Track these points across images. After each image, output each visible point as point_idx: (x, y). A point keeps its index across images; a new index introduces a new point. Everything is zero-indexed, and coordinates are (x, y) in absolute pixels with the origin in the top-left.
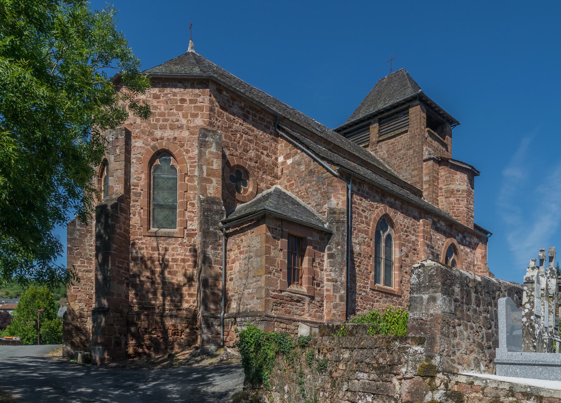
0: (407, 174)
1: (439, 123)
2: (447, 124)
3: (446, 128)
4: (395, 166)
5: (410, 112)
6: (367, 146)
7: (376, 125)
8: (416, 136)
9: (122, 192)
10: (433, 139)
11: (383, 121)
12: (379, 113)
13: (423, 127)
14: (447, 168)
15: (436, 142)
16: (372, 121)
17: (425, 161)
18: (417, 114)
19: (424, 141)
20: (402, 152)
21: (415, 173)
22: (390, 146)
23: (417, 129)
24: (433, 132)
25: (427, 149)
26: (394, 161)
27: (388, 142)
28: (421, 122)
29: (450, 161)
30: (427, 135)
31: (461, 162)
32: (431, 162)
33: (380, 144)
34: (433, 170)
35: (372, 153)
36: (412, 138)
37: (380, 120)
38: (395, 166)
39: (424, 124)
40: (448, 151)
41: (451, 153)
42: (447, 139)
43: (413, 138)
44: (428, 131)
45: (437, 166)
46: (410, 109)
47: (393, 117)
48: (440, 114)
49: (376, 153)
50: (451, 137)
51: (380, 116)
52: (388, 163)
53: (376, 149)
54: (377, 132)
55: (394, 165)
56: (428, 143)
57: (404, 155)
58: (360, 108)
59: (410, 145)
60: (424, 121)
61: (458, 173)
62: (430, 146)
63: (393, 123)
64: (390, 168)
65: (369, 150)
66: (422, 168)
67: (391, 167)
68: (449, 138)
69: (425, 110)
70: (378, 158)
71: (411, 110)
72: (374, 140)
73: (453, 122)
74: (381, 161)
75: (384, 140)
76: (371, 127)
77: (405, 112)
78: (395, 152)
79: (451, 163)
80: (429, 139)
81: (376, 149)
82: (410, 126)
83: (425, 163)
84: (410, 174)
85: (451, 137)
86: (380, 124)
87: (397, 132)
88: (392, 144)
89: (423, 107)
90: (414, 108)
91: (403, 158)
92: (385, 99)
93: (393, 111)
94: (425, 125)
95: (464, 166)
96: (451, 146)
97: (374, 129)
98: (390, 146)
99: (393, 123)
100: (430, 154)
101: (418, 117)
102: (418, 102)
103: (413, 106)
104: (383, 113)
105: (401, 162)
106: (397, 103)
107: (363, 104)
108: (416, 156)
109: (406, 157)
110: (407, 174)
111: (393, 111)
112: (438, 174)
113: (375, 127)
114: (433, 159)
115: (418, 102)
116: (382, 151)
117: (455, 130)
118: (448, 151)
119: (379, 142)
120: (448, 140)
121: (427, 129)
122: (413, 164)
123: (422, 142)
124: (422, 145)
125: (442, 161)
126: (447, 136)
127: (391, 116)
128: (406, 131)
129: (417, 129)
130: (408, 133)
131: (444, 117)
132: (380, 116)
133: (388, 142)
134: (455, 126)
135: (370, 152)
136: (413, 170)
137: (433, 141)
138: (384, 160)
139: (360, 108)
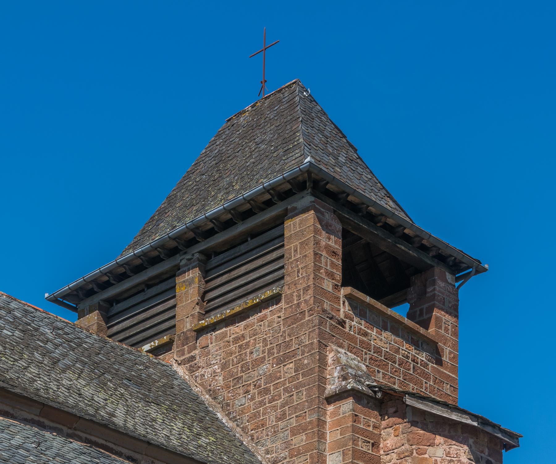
0: (278, 444)
1: (392, 267)
2: (438, 270)
3: (434, 283)
4: (246, 418)
5: (287, 234)
6: (166, 347)
7: (194, 274)
8: (303, 313)
9: (351, 400)
10: (373, 323)
11: (215, 261)
12: (200, 233)
13: (328, 285)
14: (403, 426)
15: (386, 335)
16: (181, 260)
17: (332, 399)
18: (308, 243)
19: (332, 330)
20: (265, 367)
21: (300, 440)
22: (233, 347)
23: (306, 289)
24: (368, 299)
25: (337, 361)
26: (241, 401)
27: (225, 335)
28: (317, 268)
29: (409, 401)
30: (344, 309)
31: (445, 405)
32: (347, 405)
33: (203, 340)
34: (355, 430)
35: (181, 371)
36: (293, 319)
37: (208, 255)
38: (246, 418)
39: (331, 275)
40: (439, 362)
41: (454, 369)
42: (438, 319)
43: (296, 320)
44: (349, 298)
45: (373, 418)
46: (288, 224)
47: (243, 248)
48: (407, 239)
49: (192, 370)
50: (454, 311)
51: (204, 245)
52: (225, 406)
53: (193, 358)
54: (197, 298)
55: (243, 412)
56: (352, 339)
57: (271, 378)
58: (162, 213)
59: (288, 345)
60: (334, 265)
61: (439, 439)
62: (358, 346)
63: (243, 270)
64: (230, 424)
65: (171, 359)
66: (321, 423)
67: (234, 419)
68: (447, 318)
69: (339, 227)
70: (197, 390)
71: (292, 226)
72: (188, 326)
73: (460, 267)
74: (206, 398)
75: (213, 327)
76: (179, 280)
77: (270, 234)
78: (245, 368)
79: (414, 409)
80: (356, 324)
81: (193, 358)
82: (287, 279)
83: (330, 408)
84: (287, 444)
85: (456, 316)
86: (206, 272)
87: (250, 301)
88: (236, 340)
89: (328, 217)
90: (297, 219)
91: (267, 391)
92: (230, 184)
93: (241, 228)
94: (338, 275)
95: (454, 417)
96: (455, 346)
97: (189, 286)
98: (233, 347)
99: (243, 270)
100: (345, 378)
101: (310, 252)
102: (307, 199)
103: (297, 212)
104: (210, 233)
105: (262, 403)
106: (248, 200)
107: (171, 201)
108: (302, 385)
109: (276, 386)
110: (278, 444)
111: (241, 228)
112: (375, 445)
113: (190, 283)
114: (356, 394)
115: (307, 199)
116: (209, 365)
117: (469, 291)
118: (439, 362)
119: (201, 332)
120: (441, 325)
121: (344, 291)
122: (296, 408)
123: (321, 334)
124: (322, 346)
125: (385, 402)
126: (436, 313)
127: (232, 243)
128: (276, 299)
129: (306, 289)
130: (282, 304)
131: (424, 248)
132: (204, 245)
133: (225, 335)
134: (466, 277)
135: (175, 367)
136: (295, 432)
137: (374, 333)
138: (214, 394)
139: (162, 213)
